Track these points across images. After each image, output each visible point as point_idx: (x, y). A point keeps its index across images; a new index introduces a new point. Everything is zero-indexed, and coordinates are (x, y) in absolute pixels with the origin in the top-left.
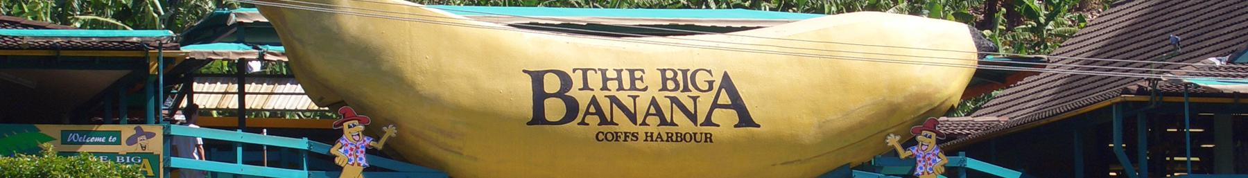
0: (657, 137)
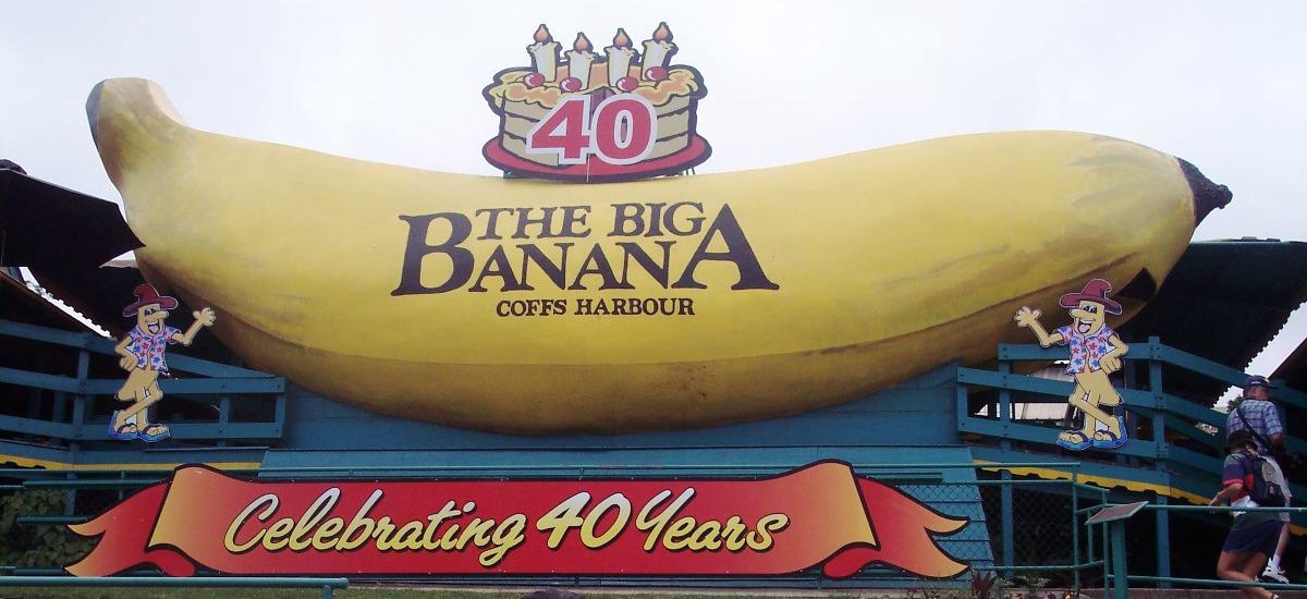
0: (598, 308)
